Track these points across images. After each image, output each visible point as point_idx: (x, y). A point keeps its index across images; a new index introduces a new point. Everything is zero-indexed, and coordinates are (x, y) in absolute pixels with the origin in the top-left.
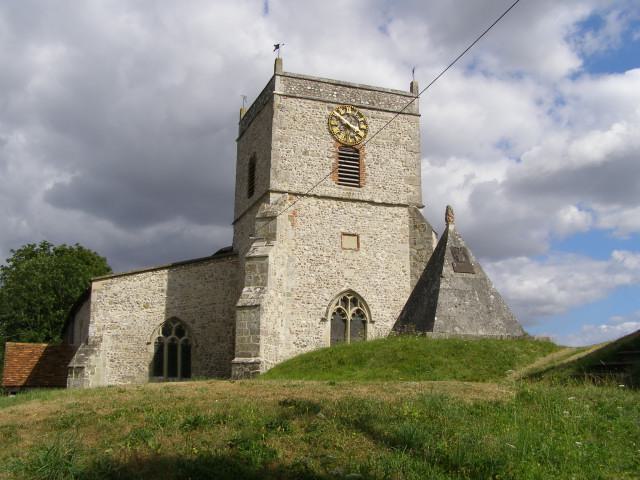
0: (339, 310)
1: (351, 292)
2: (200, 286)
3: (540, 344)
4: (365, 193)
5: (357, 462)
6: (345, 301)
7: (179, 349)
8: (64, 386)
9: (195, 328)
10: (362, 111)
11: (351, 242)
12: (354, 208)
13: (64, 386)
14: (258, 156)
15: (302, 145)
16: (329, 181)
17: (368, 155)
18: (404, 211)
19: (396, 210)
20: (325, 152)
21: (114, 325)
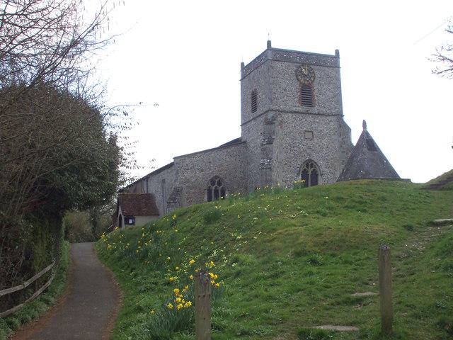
0: (305, 170)
1: (310, 160)
2: (228, 159)
3: (425, 189)
4: (315, 110)
5: (19, 80)
6: (307, 165)
7: (213, 192)
8: (330, 63)
9: (227, 180)
10: (311, 66)
11: (308, 135)
12: (310, 118)
13: (330, 63)
14: (258, 91)
15: (284, 85)
16: (297, 104)
17: (316, 88)
18: (335, 118)
19: (330, 118)
20: (294, 88)
21: (187, 181)
